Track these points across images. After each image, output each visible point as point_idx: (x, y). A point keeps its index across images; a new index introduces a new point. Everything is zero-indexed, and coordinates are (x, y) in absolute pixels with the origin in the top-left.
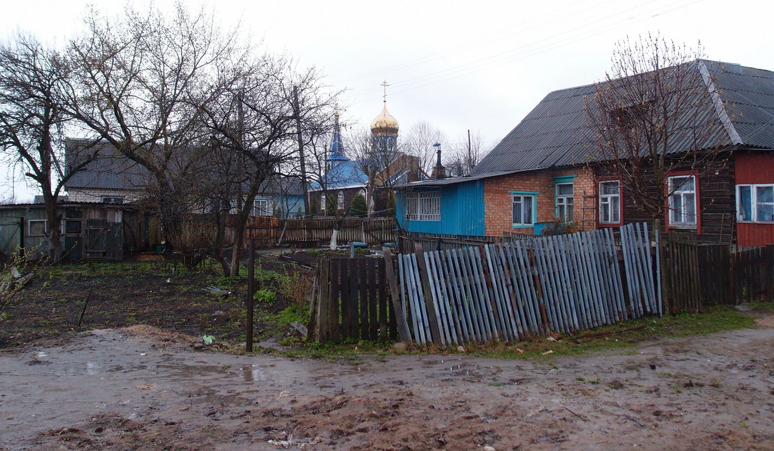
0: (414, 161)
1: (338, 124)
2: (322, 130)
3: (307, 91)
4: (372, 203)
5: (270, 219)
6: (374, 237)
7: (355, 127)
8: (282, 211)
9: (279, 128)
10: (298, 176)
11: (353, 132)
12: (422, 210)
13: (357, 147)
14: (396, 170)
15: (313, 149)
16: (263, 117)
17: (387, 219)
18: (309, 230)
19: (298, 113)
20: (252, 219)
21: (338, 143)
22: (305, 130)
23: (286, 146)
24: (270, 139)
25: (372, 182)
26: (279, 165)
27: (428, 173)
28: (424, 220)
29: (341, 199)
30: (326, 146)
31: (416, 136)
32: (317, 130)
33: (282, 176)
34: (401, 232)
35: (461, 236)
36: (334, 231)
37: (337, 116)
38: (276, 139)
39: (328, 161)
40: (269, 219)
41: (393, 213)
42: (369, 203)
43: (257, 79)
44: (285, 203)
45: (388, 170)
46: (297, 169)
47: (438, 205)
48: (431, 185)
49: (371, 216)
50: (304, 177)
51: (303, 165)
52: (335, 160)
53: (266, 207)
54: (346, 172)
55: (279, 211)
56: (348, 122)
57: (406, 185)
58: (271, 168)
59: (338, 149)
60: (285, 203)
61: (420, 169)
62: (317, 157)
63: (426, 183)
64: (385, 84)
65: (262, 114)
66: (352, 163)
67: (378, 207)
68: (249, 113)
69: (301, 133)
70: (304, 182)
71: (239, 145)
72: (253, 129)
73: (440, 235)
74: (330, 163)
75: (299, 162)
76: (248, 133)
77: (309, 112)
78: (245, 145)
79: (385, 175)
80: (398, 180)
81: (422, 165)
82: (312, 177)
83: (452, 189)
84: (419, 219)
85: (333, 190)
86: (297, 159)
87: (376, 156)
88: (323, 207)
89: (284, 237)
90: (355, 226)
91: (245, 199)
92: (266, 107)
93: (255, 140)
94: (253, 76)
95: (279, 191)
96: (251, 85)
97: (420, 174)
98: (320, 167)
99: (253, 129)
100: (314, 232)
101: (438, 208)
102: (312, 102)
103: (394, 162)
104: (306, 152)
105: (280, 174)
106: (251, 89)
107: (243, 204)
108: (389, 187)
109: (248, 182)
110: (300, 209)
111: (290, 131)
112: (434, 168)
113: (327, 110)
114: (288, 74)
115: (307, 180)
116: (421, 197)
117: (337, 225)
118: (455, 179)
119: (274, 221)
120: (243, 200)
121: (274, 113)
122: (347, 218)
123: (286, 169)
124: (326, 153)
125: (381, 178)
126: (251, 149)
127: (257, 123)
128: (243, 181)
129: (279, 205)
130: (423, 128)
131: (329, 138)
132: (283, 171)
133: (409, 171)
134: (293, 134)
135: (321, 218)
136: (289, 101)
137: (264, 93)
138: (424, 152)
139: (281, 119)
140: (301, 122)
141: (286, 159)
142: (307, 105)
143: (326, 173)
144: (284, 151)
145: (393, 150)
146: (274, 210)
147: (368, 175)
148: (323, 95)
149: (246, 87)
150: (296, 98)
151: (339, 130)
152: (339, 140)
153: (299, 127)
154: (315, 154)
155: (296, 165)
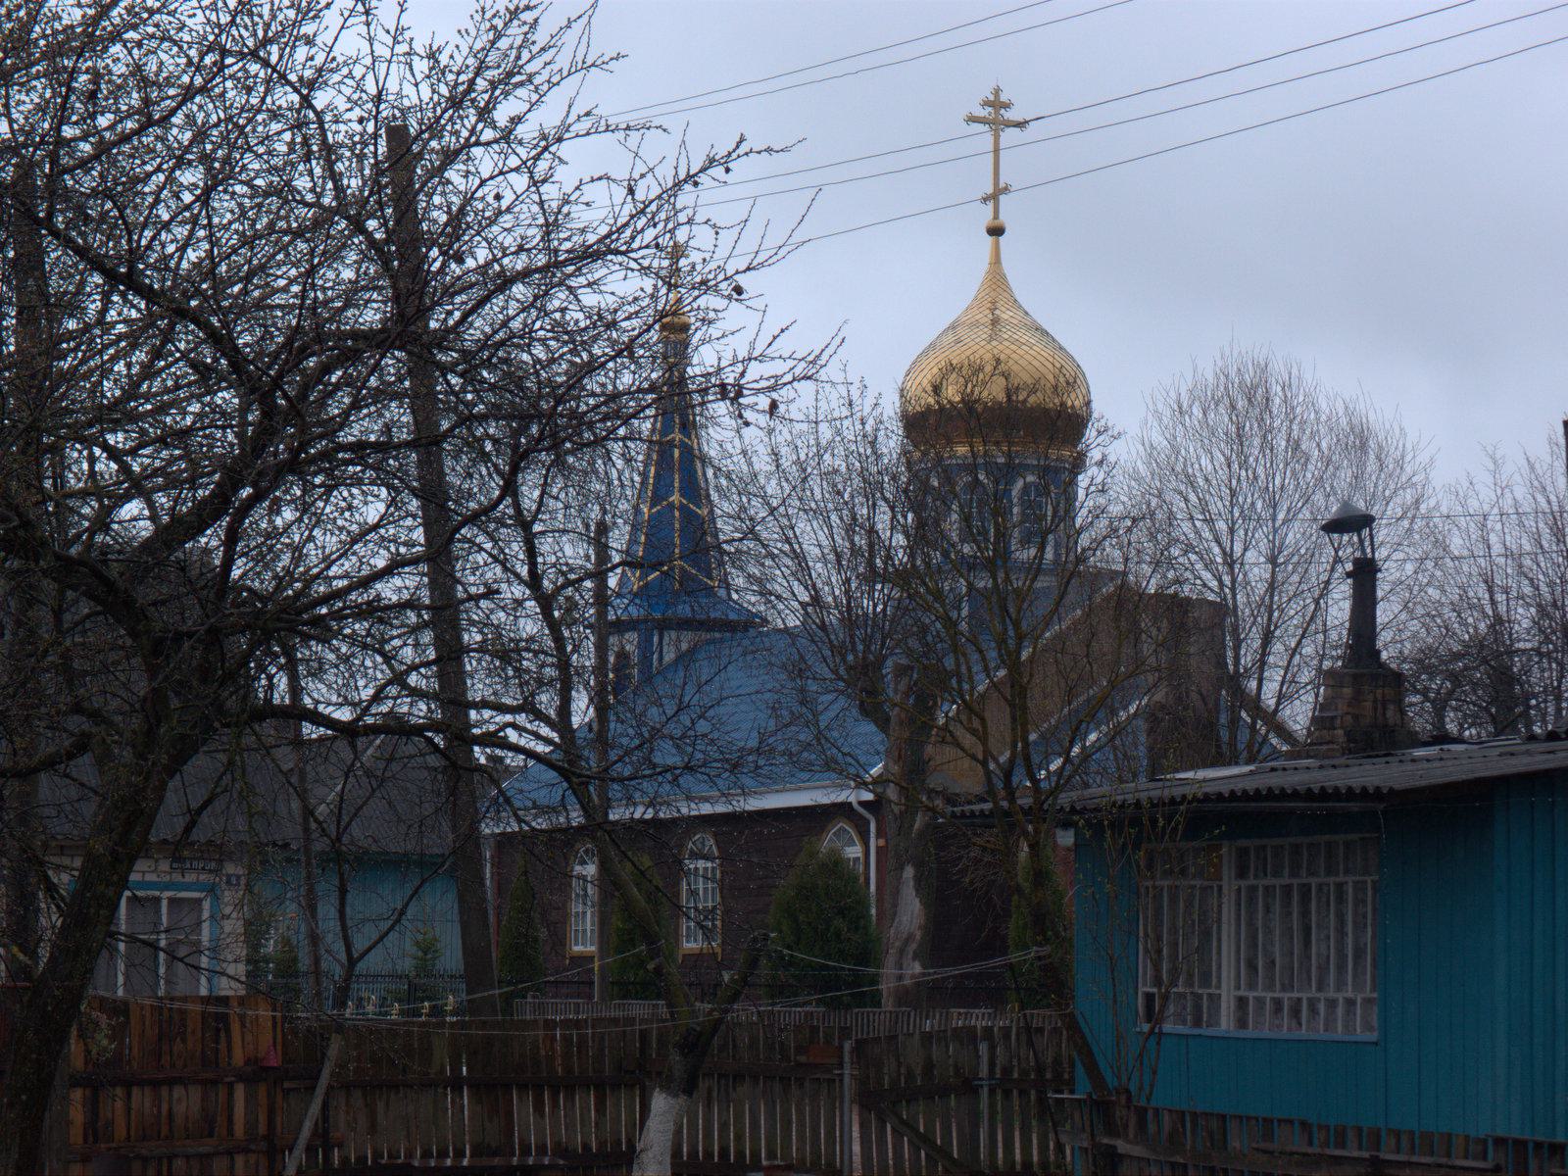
0: (1187, 633)
1: (683, 380)
2: (578, 419)
3: (485, 161)
4: (911, 912)
5: (223, 1018)
6: (927, 1140)
7: (800, 400)
8: (304, 962)
9: (297, 411)
10: (419, 730)
11: (783, 435)
12: (1252, 967)
13: (812, 537)
14: (1070, 694)
15: (516, 548)
16: (185, 338)
17: (1008, 1019)
18: (491, 1089)
19: (424, 313)
20: (103, 1019)
21: (688, 516)
22: (468, 420)
23: (349, 530)
24: (232, 480)
25: (913, 770)
26: (289, 653)
27: (1286, 713)
28: (1262, 1028)
29: (701, 879)
30: (603, 529)
31: (1208, 463)
32: (549, 423)
33: (310, 731)
34: (1103, 1109)
35: (1521, 1144)
36: (660, 1102)
37: (675, 331)
38: (277, 480)
39: (620, 627)
40: (217, 1015)
41: (1052, 984)
42: (888, 912)
43: (144, 83)
44: (327, 910)
45: (1016, 693)
46: (413, 679)
47: (1360, 927)
48: (1310, 796)
49: (903, 997)
50: (462, 737)
51: (450, 656)
52: (663, 626)
53: (204, 936)
54: (741, 702)
55: (288, 968)
56: (755, 371)
57: (1142, 789)
58: (238, 676)
59: (684, 537)
60: (327, 910)
61: (1235, 682)
62: (546, 602)
63: (1275, 781)
64: (996, 115)
65: (182, 313)
66: (782, 643)
67: (941, 940)
68: (93, 307)
69: (438, 440)
70: (456, 767)
71: (26, 524)
72: (117, 414)
73: (1375, 1138)
74: (631, 642)
75: (427, 637)
76: (88, 442)
77: (499, 301)
78: (63, 527)
79: (998, 719)
80: (1086, 755)
81: (1247, 659)
82: (512, 736)
83: (1462, 810)
84: (1226, 1023)
85: (655, 822)
86: (412, 617)
87: (938, 595)
88: (584, 939)
89: (323, 1137)
90: (793, 1071)
91: (64, 880)
92: (207, 270)
93: (137, 487)
94: (117, 59)
95: (291, 832)
96: (103, 121)
97: (1235, 721)
98: (564, 664)
99: (117, 414)
100: (523, 1109)
101: (1359, 953)
102: (514, 234)
103: (1060, 637)
104: (476, 568)
105: (295, 713)
106: (103, 149)
107: (50, 919)
108: (1025, 801)
109: (84, 767)
110: (428, 949)
111: (364, 428)
112: (1329, 678)
113: (619, 286)
114: (351, 44)
115: (480, 755)
116: (1242, 874)
117: (675, 1057)
118: (1472, 752)
119: (256, 1037)
120: (51, 889)
121: (259, 304)
122: (744, 1012)
123: (337, 688)
124: (600, 576)
125: (968, 740)
126: (105, 549)
127: (148, 372)
128: (50, 764)
129: (288, 919)
130: (1249, 409)
131: (624, 467)
132: (320, 694)
133: (1159, 696)
134: (384, 447)
135: (562, 1009)
136: (358, 227)
137: (191, 176)
138: (1257, 572)
139: (304, 353)
140: (445, 369)
141: (339, 616)
142: (482, 254)
143: (602, 710)
144: (328, 561)
145: (1049, 554)
146: (254, 961)
147: (883, 724)
148: (590, 192)
149: (68, 132)
150: (406, 203)
151: (689, 427)
152: (694, 490)
153: (423, 404)
154: (534, 581)
155: (408, 654)
